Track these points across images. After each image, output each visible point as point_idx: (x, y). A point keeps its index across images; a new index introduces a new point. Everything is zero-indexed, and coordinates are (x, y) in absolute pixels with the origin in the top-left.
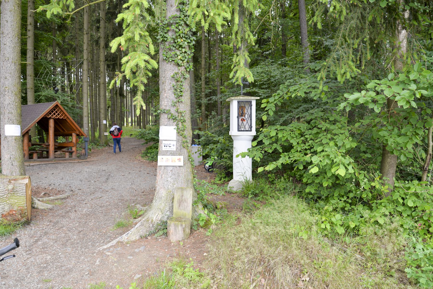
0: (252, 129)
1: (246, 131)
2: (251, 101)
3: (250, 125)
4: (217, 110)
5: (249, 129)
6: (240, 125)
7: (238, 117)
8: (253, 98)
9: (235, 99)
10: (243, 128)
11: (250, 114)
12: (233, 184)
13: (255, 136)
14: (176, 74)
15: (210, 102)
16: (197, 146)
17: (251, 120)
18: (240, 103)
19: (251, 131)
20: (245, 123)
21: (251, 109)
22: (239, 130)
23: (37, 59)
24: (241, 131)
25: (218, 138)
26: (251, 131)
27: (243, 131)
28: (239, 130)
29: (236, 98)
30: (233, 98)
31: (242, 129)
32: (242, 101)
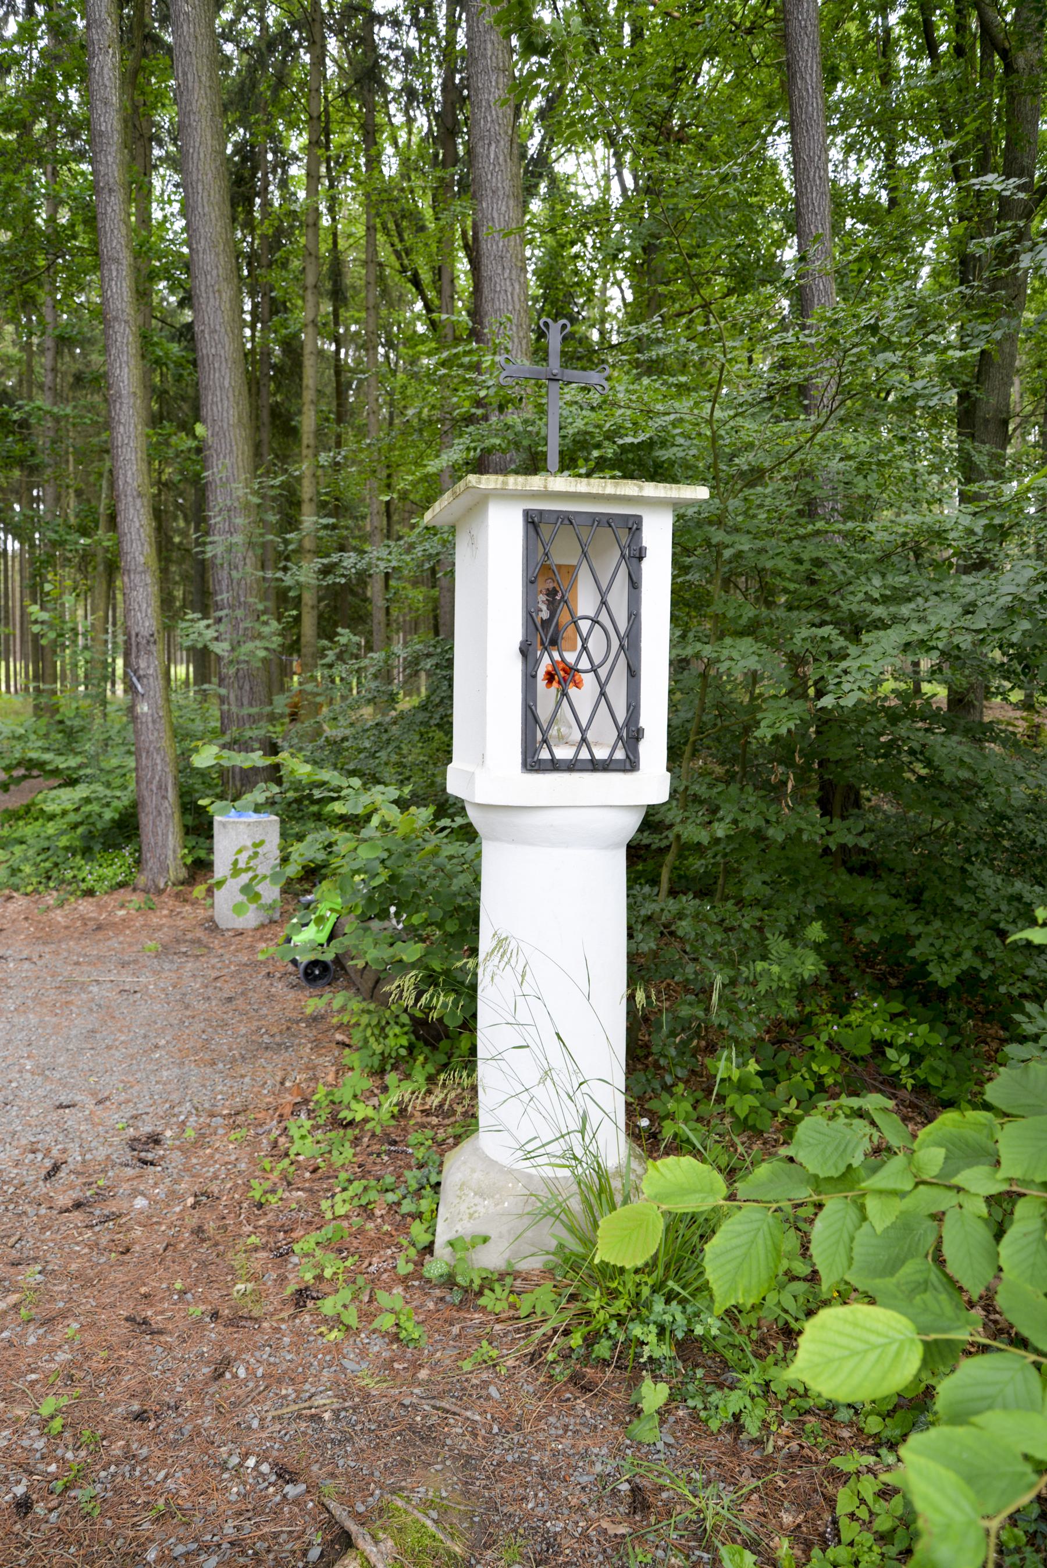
0: (643, 747)
1: (596, 766)
2: (638, 520)
3: (621, 716)
4: (371, 633)
5: (620, 755)
6: (544, 713)
7: (525, 651)
8: (651, 490)
9: (506, 495)
10: (563, 740)
11: (623, 626)
12: (485, 1207)
13: (651, 811)
14: (648, 969)
15: (330, 580)
16: (254, 817)
17: (633, 673)
18: (545, 530)
19: (631, 765)
20: (584, 695)
21: (634, 584)
22: (532, 764)
23: (694, 801)
24: (555, 766)
25: (365, 799)
26: (631, 765)
27: (572, 766)
28: (532, 764)
29: (515, 482)
30: (489, 482)
31: (563, 753)
32: (567, 519)
